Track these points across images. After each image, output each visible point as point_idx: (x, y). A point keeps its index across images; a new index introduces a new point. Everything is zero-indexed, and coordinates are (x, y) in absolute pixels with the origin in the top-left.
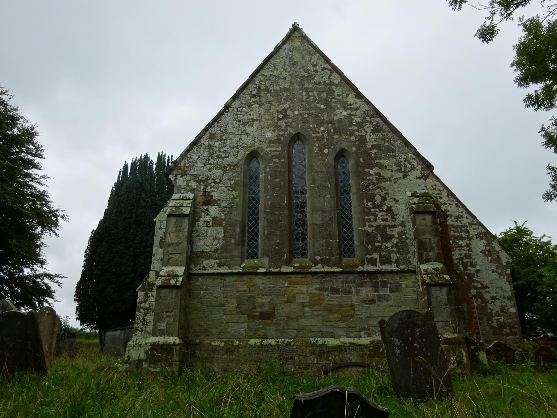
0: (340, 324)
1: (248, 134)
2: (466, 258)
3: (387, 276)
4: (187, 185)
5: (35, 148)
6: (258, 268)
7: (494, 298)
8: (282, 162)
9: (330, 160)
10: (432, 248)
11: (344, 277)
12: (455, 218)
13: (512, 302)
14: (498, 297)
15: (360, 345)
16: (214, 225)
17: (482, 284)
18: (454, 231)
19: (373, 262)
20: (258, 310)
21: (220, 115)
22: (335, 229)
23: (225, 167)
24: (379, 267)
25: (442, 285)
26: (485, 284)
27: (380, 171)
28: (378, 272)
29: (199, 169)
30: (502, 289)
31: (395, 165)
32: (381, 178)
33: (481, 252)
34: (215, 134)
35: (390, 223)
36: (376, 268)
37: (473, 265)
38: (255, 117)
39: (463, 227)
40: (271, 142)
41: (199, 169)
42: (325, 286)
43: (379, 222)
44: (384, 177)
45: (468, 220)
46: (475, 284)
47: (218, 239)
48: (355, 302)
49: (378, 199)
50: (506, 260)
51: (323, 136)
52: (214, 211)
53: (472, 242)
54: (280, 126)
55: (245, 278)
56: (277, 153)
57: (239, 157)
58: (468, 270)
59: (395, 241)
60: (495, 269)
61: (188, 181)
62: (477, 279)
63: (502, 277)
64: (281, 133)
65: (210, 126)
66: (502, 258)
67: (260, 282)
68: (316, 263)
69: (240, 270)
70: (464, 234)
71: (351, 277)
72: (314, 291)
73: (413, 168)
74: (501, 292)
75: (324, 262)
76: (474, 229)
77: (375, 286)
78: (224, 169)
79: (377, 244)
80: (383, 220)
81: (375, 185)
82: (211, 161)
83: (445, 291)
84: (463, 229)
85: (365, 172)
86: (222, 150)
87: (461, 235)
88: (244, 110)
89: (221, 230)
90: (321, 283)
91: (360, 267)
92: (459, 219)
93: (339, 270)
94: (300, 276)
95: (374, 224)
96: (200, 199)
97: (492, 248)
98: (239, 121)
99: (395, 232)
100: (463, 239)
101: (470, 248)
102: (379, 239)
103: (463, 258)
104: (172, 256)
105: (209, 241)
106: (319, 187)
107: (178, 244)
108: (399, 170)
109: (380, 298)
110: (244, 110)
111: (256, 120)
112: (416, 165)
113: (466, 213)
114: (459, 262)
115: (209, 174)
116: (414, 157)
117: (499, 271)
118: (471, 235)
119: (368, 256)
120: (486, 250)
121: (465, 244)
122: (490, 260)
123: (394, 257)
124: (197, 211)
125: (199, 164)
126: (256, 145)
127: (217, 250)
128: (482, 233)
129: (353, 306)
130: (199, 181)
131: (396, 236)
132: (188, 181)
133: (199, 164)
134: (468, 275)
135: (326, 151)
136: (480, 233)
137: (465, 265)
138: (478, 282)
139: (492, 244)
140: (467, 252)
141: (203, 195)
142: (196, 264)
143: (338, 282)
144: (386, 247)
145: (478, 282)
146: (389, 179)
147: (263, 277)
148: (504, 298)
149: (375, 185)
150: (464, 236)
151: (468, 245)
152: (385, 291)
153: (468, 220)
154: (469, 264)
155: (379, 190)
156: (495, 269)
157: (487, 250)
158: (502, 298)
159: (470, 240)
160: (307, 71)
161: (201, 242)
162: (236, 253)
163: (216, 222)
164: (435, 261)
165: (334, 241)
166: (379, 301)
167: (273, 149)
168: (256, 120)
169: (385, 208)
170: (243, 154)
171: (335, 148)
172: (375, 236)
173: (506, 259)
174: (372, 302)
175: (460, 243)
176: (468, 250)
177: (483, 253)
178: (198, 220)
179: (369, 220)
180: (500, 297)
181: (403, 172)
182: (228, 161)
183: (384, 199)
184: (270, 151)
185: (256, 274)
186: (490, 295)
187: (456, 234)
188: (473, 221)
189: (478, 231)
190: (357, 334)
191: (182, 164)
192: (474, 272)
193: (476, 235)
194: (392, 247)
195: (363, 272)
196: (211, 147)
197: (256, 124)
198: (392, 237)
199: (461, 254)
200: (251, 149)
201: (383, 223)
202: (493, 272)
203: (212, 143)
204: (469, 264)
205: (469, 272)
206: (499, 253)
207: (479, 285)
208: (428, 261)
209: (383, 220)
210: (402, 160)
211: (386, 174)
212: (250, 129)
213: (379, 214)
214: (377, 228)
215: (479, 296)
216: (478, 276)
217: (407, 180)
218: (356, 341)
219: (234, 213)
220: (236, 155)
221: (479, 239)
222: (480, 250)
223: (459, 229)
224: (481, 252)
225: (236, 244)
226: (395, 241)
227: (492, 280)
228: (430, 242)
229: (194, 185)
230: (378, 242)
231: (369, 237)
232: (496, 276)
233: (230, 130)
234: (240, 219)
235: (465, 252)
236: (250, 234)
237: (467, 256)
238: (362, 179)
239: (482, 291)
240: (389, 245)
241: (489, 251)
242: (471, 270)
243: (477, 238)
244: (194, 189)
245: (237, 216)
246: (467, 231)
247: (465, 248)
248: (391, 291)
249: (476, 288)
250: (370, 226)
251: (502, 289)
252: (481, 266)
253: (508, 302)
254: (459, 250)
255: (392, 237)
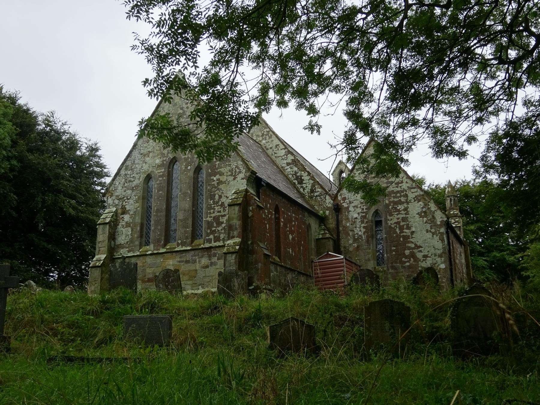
0: (189, 282)
1: (146, 163)
2: (403, 222)
3: (217, 249)
4: (113, 203)
5: (432, 44)
6: (147, 251)
7: (425, 256)
8: (164, 180)
9: (191, 174)
10: (236, 229)
11: (193, 252)
12: (396, 184)
13: (443, 259)
14: (429, 256)
15: (196, 294)
16: (127, 227)
17: (416, 245)
18: (394, 197)
19: (209, 241)
20: (147, 277)
21: (131, 152)
22: (190, 222)
23: (133, 188)
24: (213, 244)
25: (232, 253)
26: (418, 244)
27: (220, 177)
28: (211, 248)
29: (119, 191)
30: (434, 247)
31: (230, 171)
32: (220, 182)
33: (418, 214)
34: (128, 166)
35: (223, 213)
36: (211, 245)
37: (408, 228)
38: (150, 150)
39: (402, 192)
40: (159, 166)
41: (119, 191)
42: (182, 259)
43: (216, 214)
44: (222, 181)
45: (408, 185)
46: (409, 245)
47: (128, 235)
48: (197, 268)
49: (217, 197)
50: (441, 220)
51: (188, 157)
52: (127, 218)
53: (410, 205)
54: (164, 154)
55: (141, 258)
56: (161, 173)
57: (141, 180)
58: (404, 232)
59: (224, 225)
60: (429, 229)
61: (114, 200)
62: (411, 240)
63: (435, 236)
64: (165, 159)
65: (125, 161)
66: (437, 218)
67: (149, 260)
68: (178, 245)
69: (138, 253)
70: (403, 199)
71: (197, 252)
72: (176, 263)
73: (240, 172)
74: (433, 250)
75: (183, 244)
76: (412, 193)
77: (210, 257)
78: (132, 189)
79: (214, 229)
80: (218, 212)
81: (215, 187)
82: (126, 185)
83: (234, 256)
84: (402, 194)
85: (211, 179)
86: (132, 176)
87: (400, 200)
88: (145, 145)
89: (130, 229)
90: (180, 258)
91: (202, 246)
92: (400, 185)
93: (189, 248)
94: (169, 254)
95: (213, 215)
96: (120, 211)
97: (429, 208)
98: (142, 154)
99: (224, 220)
100: (401, 203)
101: (407, 211)
102: (215, 225)
103: (400, 222)
104: (101, 249)
105: (123, 237)
106: (183, 194)
107: (103, 241)
108: (231, 175)
109: (212, 264)
110: (145, 145)
111: (151, 152)
112: (242, 169)
113: (406, 178)
114: (396, 226)
115: (124, 193)
116: (242, 163)
117: (433, 230)
118: (409, 198)
119: (207, 238)
120: (422, 212)
121: (403, 208)
122: (425, 221)
123: (222, 236)
124: (118, 218)
125: (120, 188)
126: (151, 170)
127: (128, 242)
128: (420, 195)
129: (196, 270)
130: (119, 199)
131: (225, 222)
132: (114, 200)
133: (120, 188)
134: (404, 237)
135: (189, 168)
136: (418, 195)
137: (401, 229)
138: (412, 243)
139: (429, 205)
140: (404, 216)
141: (122, 208)
142: (117, 252)
143: (189, 256)
144: (218, 230)
145: (412, 243)
146: (225, 182)
147: (151, 257)
148: (435, 255)
149: (215, 187)
150: (403, 200)
151: (406, 209)
152: (215, 259)
153: (408, 185)
154: (405, 227)
155: (218, 191)
156: (429, 229)
157: (424, 212)
158: (433, 255)
159: (408, 203)
160: (182, 109)
161: (120, 239)
162: (137, 243)
163: (128, 225)
164: (237, 237)
165: (189, 229)
166: (211, 266)
167: (159, 171)
168: (151, 152)
169: (220, 203)
170: (143, 176)
171: (195, 164)
172: (213, 223)
173: (441, 218)
174: (207, 267)
175: (398, 208)
176: (406, 214)
177: (420, 215)
178: (118, 225)
179: (210, 213)
180: (432, 255)
181: (234, 176)
182: (135, 183)
183: (220, 197)
184: (158, 173)
185: (146, 255)
186: (422, 254)
187: (396, 200)
188: (412, 185)
189: (416, 194)
190: (197, 287)
191: (111, 189)
192: (409, 234)
193: (414, 198)
194: (222, 230)
195: (203, 248)
196: (126, 175)
197: (151, 155)
198: (222, 223)
199: (398, 219)
200: (147, 173)
201: (218, 214)
202: (427, 232)
203: (126, 172)
204: (405, 227)
205: (404, 234)
206: (434, 213)
207: (413, 246)
208: (233, 237)
209: (218, 212)
210: (234, 167)
211: (223, 178)
212: (147, 159)
213: (216, 208)
214: (214, 217)
215: (413, 255)
216: (412, 238)
217: (235, 181)
218: (196, 292)
219: (137, 218)
220: (139, 179)
221: (417, 202)
222: (417, 212)
223: (398, 195)
224: (418, 214)
225: (137, 237)
226: (224, 225)
227: (425, 240)
228: (236, 225)
229: (117, 202)
230: (214, 227)
231: (209, 224)
232: (429, 235)
233: (136, 162)
234: (140, 221)
235: (402, 216)
236: (147, 230)
237: (404, 219)
238: (209, 185)
239: (415, 251)
240: (220, 229)
241: (425, 212)
242: (407, 232)
243: (415, 201)
244: (117, 205)
245: (138, 219)
246: (406, 196)
247: (403, 212)
248: (218, 259)
249: (409, 248)
250: (210, 217)
251: (434, 247)
252: (416, 227)
253: (438, 259)
254: (397, 215)
255: (222, 223)
